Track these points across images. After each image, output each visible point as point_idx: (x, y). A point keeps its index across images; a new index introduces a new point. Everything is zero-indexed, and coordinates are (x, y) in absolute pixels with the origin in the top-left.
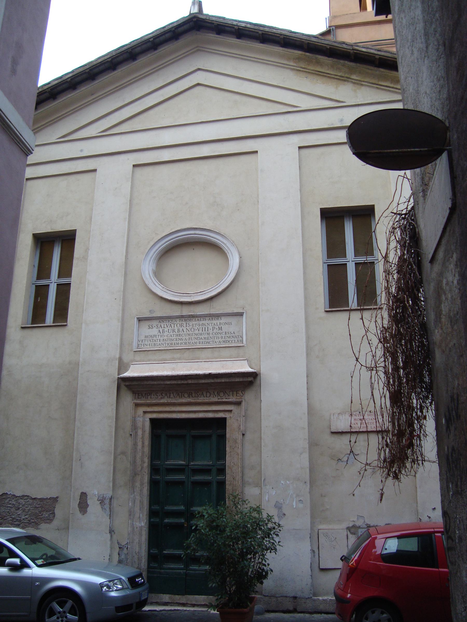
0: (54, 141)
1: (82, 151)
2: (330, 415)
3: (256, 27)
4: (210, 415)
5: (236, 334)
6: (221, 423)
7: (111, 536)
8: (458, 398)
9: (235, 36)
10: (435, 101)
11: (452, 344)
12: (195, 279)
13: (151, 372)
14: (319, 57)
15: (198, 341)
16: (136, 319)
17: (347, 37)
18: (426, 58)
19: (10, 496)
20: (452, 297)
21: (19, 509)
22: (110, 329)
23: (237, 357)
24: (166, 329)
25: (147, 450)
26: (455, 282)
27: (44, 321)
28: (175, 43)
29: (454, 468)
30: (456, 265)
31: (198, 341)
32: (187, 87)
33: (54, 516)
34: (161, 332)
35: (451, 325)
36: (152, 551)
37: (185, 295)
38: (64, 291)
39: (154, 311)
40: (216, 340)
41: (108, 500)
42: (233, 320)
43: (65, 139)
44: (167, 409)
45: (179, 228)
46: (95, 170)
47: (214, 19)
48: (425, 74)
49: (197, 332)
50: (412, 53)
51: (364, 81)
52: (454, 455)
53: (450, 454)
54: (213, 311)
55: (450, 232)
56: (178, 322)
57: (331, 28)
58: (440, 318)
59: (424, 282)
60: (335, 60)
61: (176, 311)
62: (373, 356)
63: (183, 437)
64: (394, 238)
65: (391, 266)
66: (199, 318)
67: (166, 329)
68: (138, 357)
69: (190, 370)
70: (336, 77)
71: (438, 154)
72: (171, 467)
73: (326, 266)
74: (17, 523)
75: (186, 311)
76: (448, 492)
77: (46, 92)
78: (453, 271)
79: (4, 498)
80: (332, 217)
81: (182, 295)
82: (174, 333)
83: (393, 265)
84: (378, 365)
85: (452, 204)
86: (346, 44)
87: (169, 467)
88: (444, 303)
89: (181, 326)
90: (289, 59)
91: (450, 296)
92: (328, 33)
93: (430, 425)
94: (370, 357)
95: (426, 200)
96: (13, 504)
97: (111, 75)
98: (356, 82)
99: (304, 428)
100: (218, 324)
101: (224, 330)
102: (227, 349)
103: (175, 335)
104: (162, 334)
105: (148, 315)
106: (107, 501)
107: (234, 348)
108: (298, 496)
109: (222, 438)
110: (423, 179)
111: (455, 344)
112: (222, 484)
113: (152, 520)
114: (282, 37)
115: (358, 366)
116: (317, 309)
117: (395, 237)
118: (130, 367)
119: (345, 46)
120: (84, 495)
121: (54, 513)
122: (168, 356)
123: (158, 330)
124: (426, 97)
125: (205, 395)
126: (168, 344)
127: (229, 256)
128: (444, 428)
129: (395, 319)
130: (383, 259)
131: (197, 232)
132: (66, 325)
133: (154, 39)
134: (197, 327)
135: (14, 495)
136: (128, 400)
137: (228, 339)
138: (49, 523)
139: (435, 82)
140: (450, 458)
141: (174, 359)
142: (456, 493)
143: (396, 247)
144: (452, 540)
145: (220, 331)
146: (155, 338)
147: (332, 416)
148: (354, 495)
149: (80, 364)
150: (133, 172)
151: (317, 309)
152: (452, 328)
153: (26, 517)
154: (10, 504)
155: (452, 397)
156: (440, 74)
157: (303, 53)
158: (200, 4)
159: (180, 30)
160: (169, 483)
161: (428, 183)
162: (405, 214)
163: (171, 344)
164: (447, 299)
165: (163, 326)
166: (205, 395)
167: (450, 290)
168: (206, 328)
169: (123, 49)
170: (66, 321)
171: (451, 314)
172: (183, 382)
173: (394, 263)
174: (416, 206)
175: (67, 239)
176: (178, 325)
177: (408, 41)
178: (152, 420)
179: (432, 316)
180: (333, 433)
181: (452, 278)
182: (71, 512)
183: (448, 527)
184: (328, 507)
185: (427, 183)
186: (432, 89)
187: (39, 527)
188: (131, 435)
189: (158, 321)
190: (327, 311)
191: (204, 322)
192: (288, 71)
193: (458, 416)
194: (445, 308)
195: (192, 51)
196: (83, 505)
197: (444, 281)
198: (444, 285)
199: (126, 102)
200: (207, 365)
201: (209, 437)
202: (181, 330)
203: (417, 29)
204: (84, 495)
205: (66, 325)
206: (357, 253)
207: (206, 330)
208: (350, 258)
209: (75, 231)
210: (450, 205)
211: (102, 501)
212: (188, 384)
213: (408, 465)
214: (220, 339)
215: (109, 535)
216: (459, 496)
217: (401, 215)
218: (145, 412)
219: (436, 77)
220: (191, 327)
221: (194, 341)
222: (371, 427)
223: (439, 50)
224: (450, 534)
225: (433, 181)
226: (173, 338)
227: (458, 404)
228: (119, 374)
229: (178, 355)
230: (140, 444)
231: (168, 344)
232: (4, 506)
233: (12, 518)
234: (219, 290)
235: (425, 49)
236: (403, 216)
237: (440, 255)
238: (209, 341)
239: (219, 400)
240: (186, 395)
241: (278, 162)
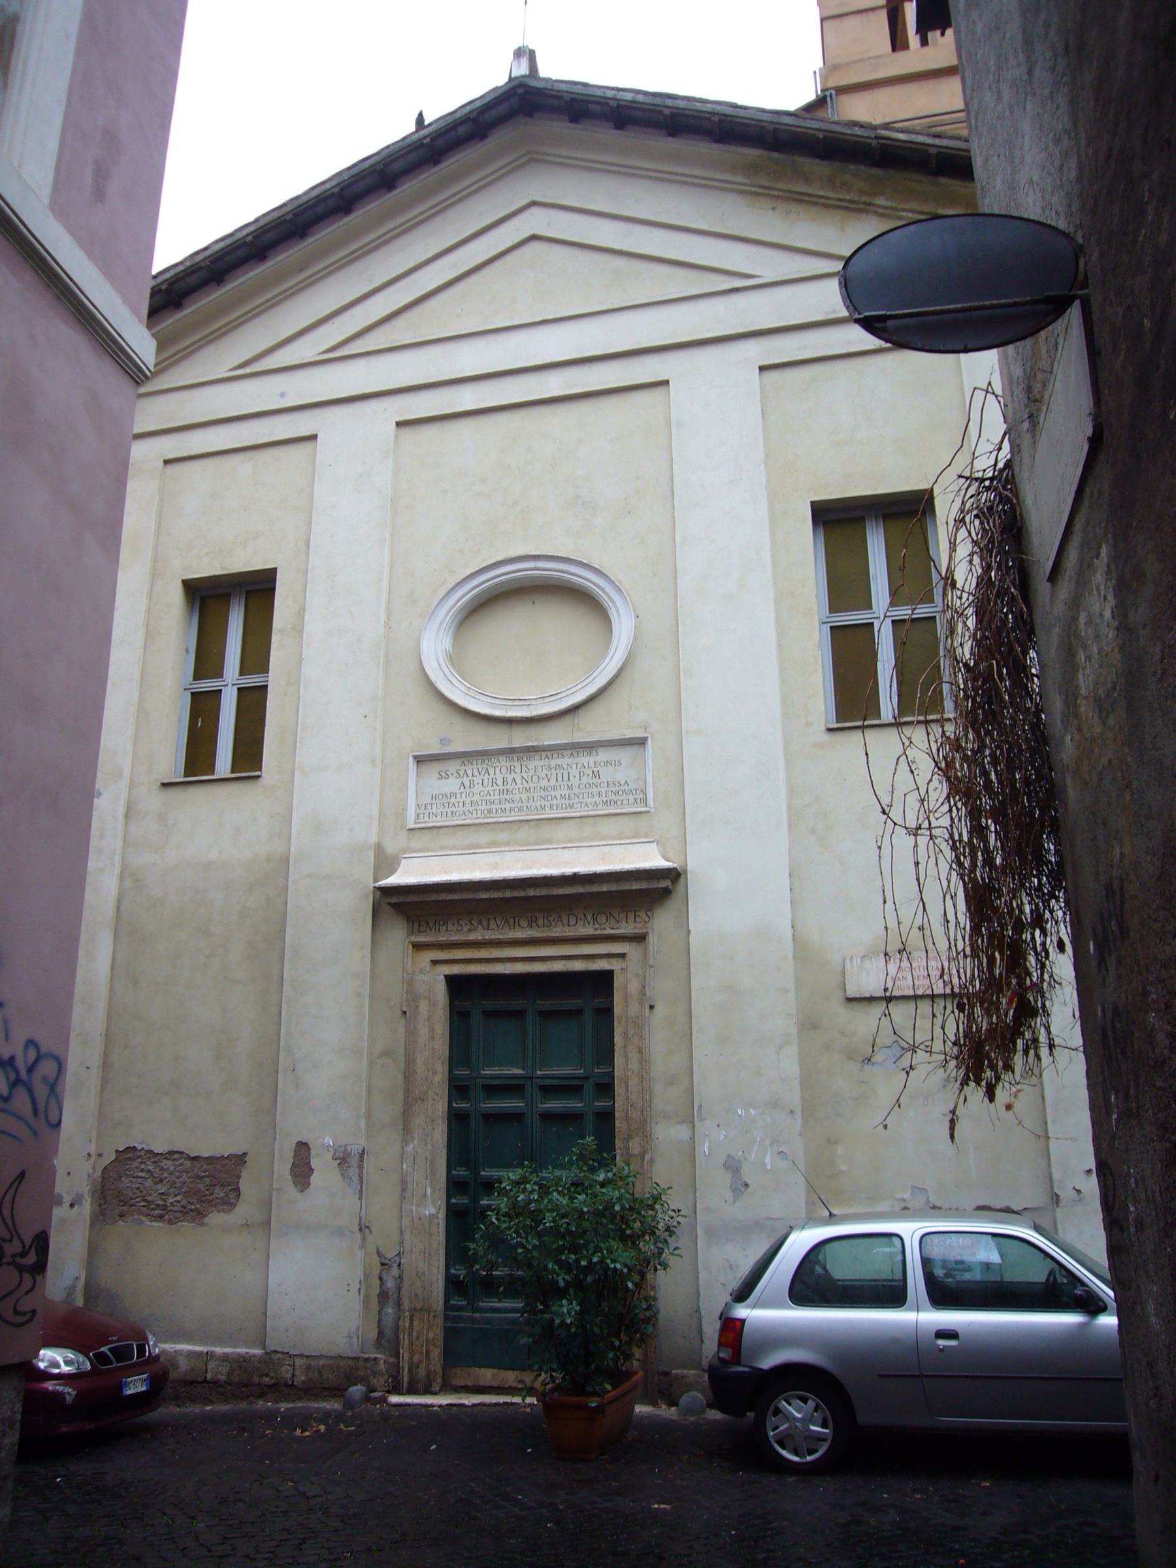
0: (220, 376)
1: (283, 395)
2: (844, 961)
3: (658, 101)
4: (578, 966)
5: (632, 786)
6: (603, 982)
7: (364, 1239)
8: (1122, 888)
9: (612, 124)
10: (1053, 193)
11: (1104, 761)
12: (534, 667)
13: (446, 873)
14: (800, 160)
15: (548, 804)
16: (411, 759)
17: (863, 111)
18: (1029, 98)
19: (142, 1153)
20: (1100, 651)
21: (161, 1181)
22: (360, 787)
23: (634, 837)
24: (477, 780)
25: (442, 1045)
26: (1108, 614)
27: (212, 770)
28: (480, 145)
29: (1120, 1056)
30: (1108, 572)
31: (548, 804)
32: (509, 244)
33: (238, 1196)
34: (467, 784)
35: (1100, 717)
36: (453, 1271)
37: (516, 703)
38: (253, 702)
39: (451, 741)
40: (586, 800)
41: (356, 1159)
42: (624, 756)
43: (246, 372)
44: (483, 953)
45: (500, 558)
46: (314, 437)
47: (562, 87)
48: (1027, 138)
49: (544, 783)
50: (999, 98)
51: (903, 210)
52: (1118, 1025)
53: (1109, 1025)
54: (578, 738)
55: (1091, 496)
56: (503, 762)
57: (828, 93)
58: (1076, 706)
59: (1037, 631)
60: (836, 164)
61: (499, 739)
62: (922, 801)
63: (519, 1014)
64: (967, 534)
65: (961, 598)
66: (549, 754)
67: (477, 780)
68: (416, 843)
69: (530, 868)
70: (839, 203)
71: (1059, 306)
72: (494, 1082)
73: (826, 629)
74: (157, 1212)
75: (520, 738)
76: (1108, 1113)
77: (200, 269)
78: (1102, 588)
79: (129, 1159)
80: (837, 520)
81: (510, 703)
82: (495, 787)
83: (965, 596)
84: (934, 823)
85: (1095, 427)
86: (862, 126)
87: (487, 1082)
88: (1083, 669)
89: (511, 770)
90: (733, 169)
91: (1095, 650)
92: (820, 103)
93: (1063, 966)
94: (913, 801)
95: (1038, 436)
96: (149, 1171)
97: (341, 223)
98: (885, 211)
99: (786, 991)
100: (592, 764)
101: (604, 778)
102: (613, 819)
103: (497, 793)
104: (468, 790)
105: (436, 749)
106: (354, 1161)
107: (626, 818)
108: (775, 1142)
109: (606, 1013)
110: (1029, 389)
111: (1110, 761)
112: (606, 1117)
113: (453, 1201)
114: (716, 119)
115: (890, 824)
116: (809, 724)
117: (969, 532)
118: (399, 864)
119: (857, 131)
120: (303, 1148)
121: (238, 1189)
122: (483, 837)
123: (459, 781)
124: (1031, 192)
125: (565, 922)
126: (482, 812)
127: (613, 613)
128: (1094, 963)
129: (971, 719)
130: (942, 582)
131: (541, 564)
132: (259, 777)
133: (433, 140)
134: (545, 772)
135: (151, 1152)
136: (397, 936)
137: (614, 797)
138: (228, 1212)
139: (1051, 148)
140: (1109, 1032)
141: (494, 844)
142: (1127, 1115)
143: (972, 554)
144: (1122, 1229)
145: (595, 781)
146: (453, 800)
147: (848, 961)
148: (886, 1127)
149: (291, 859)
150: (396, 437)
151: (809, 724)
152: (1104, 723)
153: (178, 1198)
154: (142, 1170)
155: (1109, 889)
156: (1061, 126)
157: (764, 153)
158: (532, 56)
159: (491, 115)
160: (492, 1118)
161: (1042, 397)
162: (992, 479)
163: (490, 811)
164: (1089, 658)
165: (470, 773)
166: (565, 922)
167: (1097, 636)
168: (566, 775)
169: (366, 165)
170: (260, 770)
171: (1100, 691)
172: (516, 894)
173: (966, 589)
174: (1017, 458)
175: (257, 589)
176: (504, 770)
177: (988, 71)
178: (451, 980)
179: (1057, 704)
180: (850, 1000)
181: (1101, 606)
182: (275, 1186)
183: (1110, 1199)
184: (844, 1168)
185: (1038, 397)
186: (1044, 168)
187: (206, 1220)
188: (405, 1013)
189: (459, 762)
190: (830, 730)
191: (559, 761)
192: (732, 197)
193: (1124, 932)
194: (1085, 682)
195: (516, 163)
196: (302, 1171)
197: (1083, 618)
198: (1082, 626)
199: (377, 284)
200: (568, 855)
201: (579, 1012)
202: (510, 781)
203: (1008, 35)
204: (303, 1148)
205: (259, 777)
206: (896, 596)
207: (566, 778)
208: (881, 609)
209: (274, 571)
210: (1089, 433)
211: (343, 1159)
212: (527, 898)
213: (1018, 1060)
214: (596, 798)
215: (358, 1235)
216: (1134, 1122)
217: (983, 480)
218: (435, 962)
219: (1051, 136)
220: (531, 773)
221: (538, 804)
222: (939, 989)
223: (1057, 68)
224: (1114, 1214)
225: (1050, 388)
226: (493, 798)
227: (1122, 902)
228: (376, 881)
229: (504, 836)
230: (424, 1032)
231: (482, 812)
232: (129, 1176)
233: (146, 1201)
234: (592, 689)
235: (1025, 77)
236: (987, 483)
237: (1071, 558)
238: (571, 802)
239: (598, 932)
240: (524, 923)
241: (717, 401)
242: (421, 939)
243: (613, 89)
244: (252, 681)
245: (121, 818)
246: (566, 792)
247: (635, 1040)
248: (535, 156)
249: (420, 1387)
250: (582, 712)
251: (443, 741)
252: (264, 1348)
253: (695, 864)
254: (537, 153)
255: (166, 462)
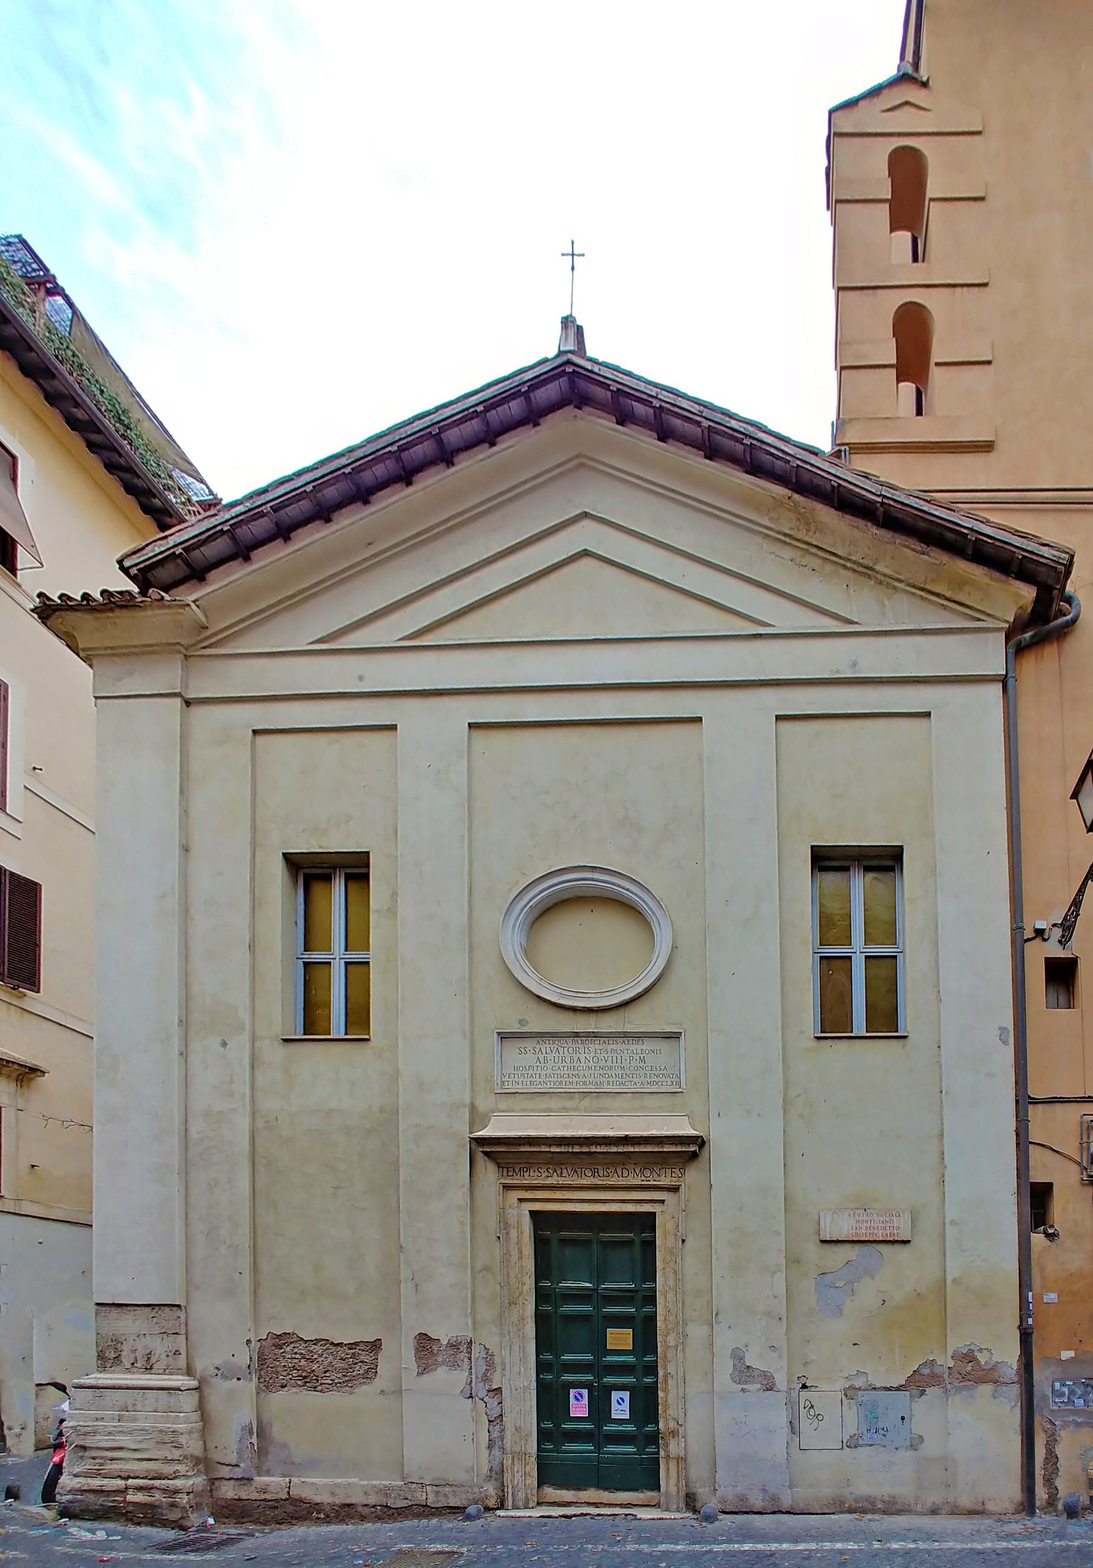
12: (590, 962)
25: (530, 1264)
42: (664, 1046)
43: (328, 647)
44: (559, 1195)
46: (393, 728)
54: (628, 1028)
57: (843, 448)
89: (575, 1051)
106: (463, 1348)
122: (554, 1103)
131: (596, 876)
136: (489, 1173)
151: (802, 1032)
163: (561, 1083)
175: (355, 869)
180: (823, 1242)
191: (614, 1047)
218: (520, 1200)
220: (593, 1054)
234: (640, 989)
242: (509, 1181)
243: (656, 385)
244: (355, 956)
245: (247, 1067)
246: (619, 1072)
247: (672, 1264)
248: (584, 460)
249: (521, 1504)
250: (631, 1006)
251: (521, 1022)
252: (403, 1478)
253: (716, 1134)
254: (590, 459)
255: (255, 732)
